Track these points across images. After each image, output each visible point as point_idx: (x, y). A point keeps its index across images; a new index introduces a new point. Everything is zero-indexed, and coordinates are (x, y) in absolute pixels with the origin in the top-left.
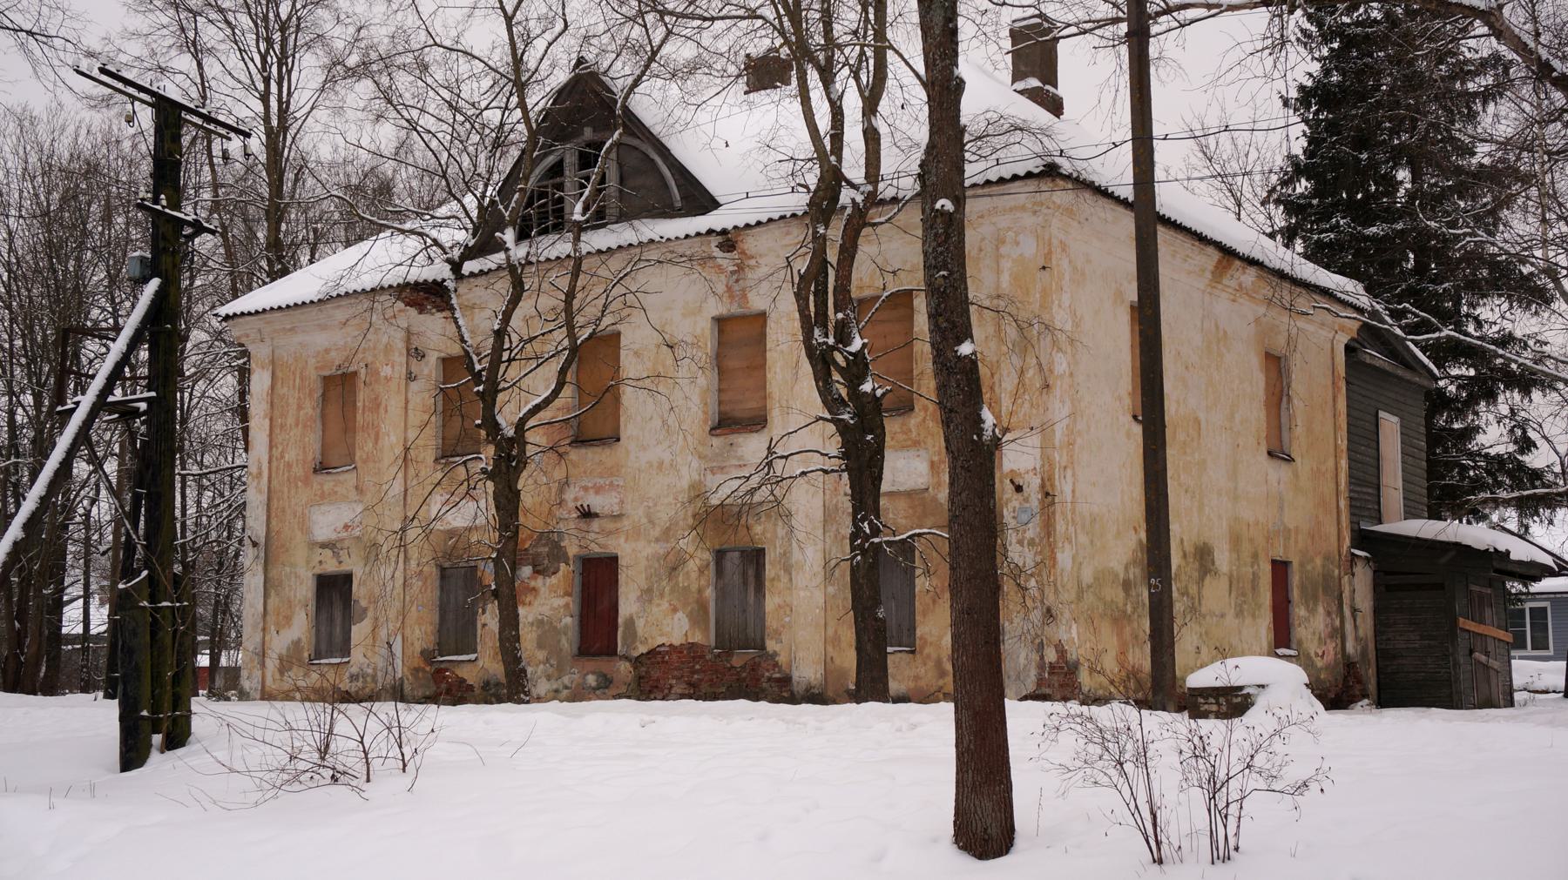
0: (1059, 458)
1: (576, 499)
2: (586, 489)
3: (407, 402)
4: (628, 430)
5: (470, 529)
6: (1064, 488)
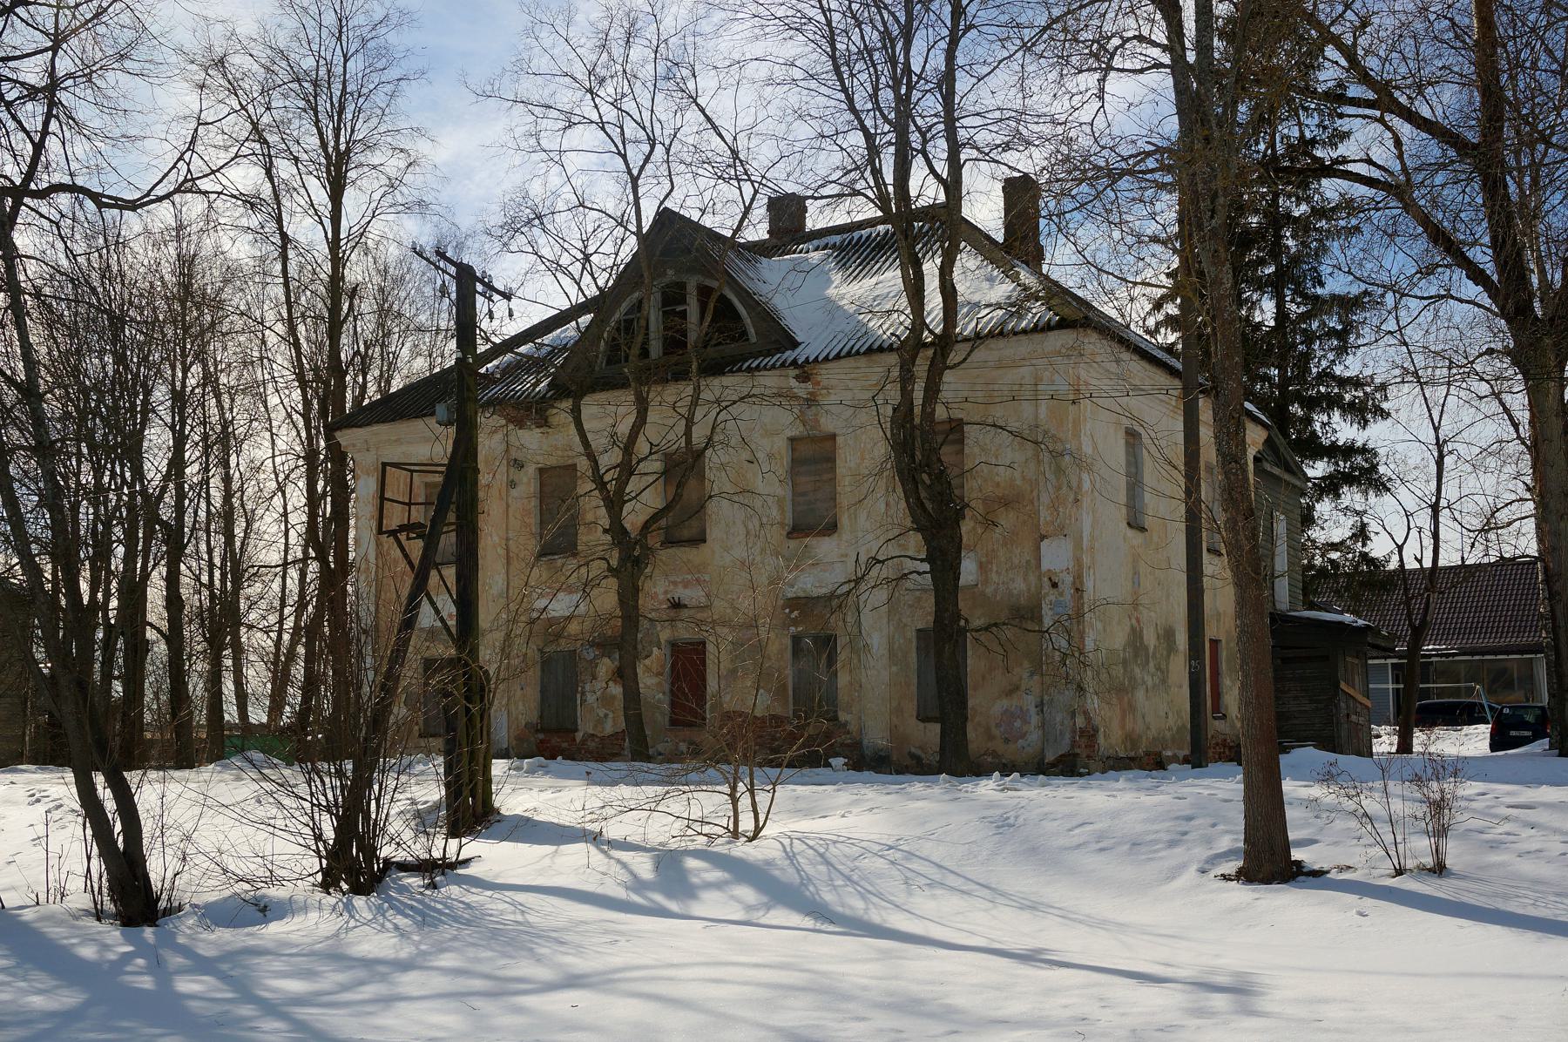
0: (1086, 560)
1: (666, 592)
2: (675, 583)
3: (508, 506)
4: (714, 533)
5: (569, 619)
6: (1089, 585)
